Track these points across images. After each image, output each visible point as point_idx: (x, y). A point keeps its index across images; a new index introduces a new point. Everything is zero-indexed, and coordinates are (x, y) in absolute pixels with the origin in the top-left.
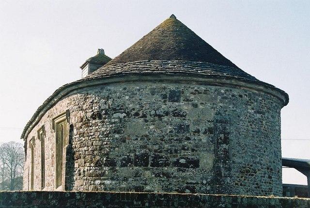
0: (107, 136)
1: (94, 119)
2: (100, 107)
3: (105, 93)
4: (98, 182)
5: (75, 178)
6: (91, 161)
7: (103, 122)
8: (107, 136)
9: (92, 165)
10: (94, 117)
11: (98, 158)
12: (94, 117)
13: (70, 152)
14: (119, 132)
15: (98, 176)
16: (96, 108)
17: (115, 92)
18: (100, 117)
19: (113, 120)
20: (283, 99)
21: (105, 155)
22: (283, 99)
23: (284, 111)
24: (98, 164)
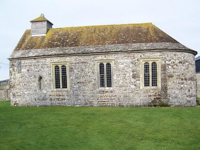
23: (53, 26)
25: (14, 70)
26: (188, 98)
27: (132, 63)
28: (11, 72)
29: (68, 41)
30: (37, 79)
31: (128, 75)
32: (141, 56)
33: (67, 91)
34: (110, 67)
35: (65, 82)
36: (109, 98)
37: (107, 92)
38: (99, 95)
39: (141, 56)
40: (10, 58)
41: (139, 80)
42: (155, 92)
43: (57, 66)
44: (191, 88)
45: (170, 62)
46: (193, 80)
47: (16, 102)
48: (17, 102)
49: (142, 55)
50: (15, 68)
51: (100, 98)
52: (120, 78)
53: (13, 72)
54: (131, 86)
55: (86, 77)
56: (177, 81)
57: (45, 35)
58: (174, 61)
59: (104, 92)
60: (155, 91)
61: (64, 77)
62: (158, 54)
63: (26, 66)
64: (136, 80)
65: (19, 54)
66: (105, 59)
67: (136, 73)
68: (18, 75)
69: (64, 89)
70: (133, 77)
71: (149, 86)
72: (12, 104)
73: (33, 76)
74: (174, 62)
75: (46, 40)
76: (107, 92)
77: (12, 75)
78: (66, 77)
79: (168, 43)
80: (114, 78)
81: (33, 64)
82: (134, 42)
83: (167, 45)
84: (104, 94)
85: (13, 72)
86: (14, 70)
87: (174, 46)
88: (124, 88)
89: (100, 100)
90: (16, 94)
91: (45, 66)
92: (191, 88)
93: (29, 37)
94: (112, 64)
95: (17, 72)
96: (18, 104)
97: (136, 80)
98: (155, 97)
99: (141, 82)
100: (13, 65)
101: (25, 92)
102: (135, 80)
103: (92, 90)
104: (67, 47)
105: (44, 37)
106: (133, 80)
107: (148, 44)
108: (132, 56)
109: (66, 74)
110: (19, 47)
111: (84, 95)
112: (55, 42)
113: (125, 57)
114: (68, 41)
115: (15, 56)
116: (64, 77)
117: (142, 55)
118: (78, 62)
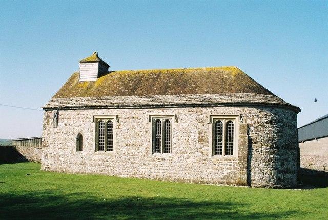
0: (276, 133)
1: (268, 123)
2: (272, 118)
3: (273, 111)
4: (271, 156)
5: (253, 153)
6: (267, 146)
7: (273, 126)
8: (276, 133)
9: (268, 147)
10: (267, 123)
11: (271, 144)
12: (267, 123)
13: (250, 142)
14: (281, 133)
15: (272, 153)
16: (269, 119)
17: (279, 112)
18: (271, 124)
19: (278, 126)
20: (297, 110)
21: (275, 143)
22: (297, 110)
23: (299, 115)
24: (271, 147)
25: (48, 123)
26: (280, 176)
27: (198, 121)
28: (44, 126)
29: (121, 88)
30: (76, 136)
31: (192, 137)
32: (211, 112)
33: (112, 156)
34: (170, 125)
35: (231, 149)
36: (165, 168)
37: (163, 159)
38: (153, 163)
39: (211, 112)
40: (45, 106)
41: (207, 145)
42: (230, 163)
43: (110, 121)
44: (287, 160)
45: (253, 122)
46: (291, 149)
47: (48, 165)
48: (49, 166)
49: (213, 111)
50: (50, 120)
51: (153, 167)
52: (180, 141)
53: (48, 126)
54: (196, 153)
55: (137, 137)
56: (263, 149)
57: (96, 79)
58: (259, 120)
59: (159, 159)
60: (230, 161)
61: (110, 136)
62: (234, 110)
63: (64, 118)
64: (204, 146)
65: (56, 104)
66: (163, 114)
67: (203, 135)
68: (53, 130)
69: (228, 156)
70: (199, 141)
71: (221, 154)
72: (43, 168)
73: (71, 133)
74: (258, 123)
75: (95, 87)
76: (163, 159)
77: (45, 129)
78: (112, 136)
79: (253, 94)
80: (174, 140)
81: (72, 116)
82: (206, 92)
83: (252, 97)
84: (159, 161)
85: (48, 126)
86: (48, 123)
87: (262, 99)
88: (186, 156)
89: (154, 170)
90: (49, 155)
91: (87, 119)
92: (287, 160)
93: (76, 81)
94: (172, 121)
95: (52, 126)
96: (50, 168)
97: (204, 146)
98: (229, 171)
99: (209, 148)
100: (48, 116)
101: (60, 154)
102: (202, 145)
103: (144, 156)
104: (118, 96)
105: (94, 82)
106: (199, 145)
107: (224, 96)
108: (199, 110)
109: (112, 133)
110: (61, 94)
111: (133, 161)
112: (105, 88)
113: (189, 113)
114: (121, 88)
115: (52, 105)
116: (110, 136)
117: (213, 111)
118: (127, 117)
